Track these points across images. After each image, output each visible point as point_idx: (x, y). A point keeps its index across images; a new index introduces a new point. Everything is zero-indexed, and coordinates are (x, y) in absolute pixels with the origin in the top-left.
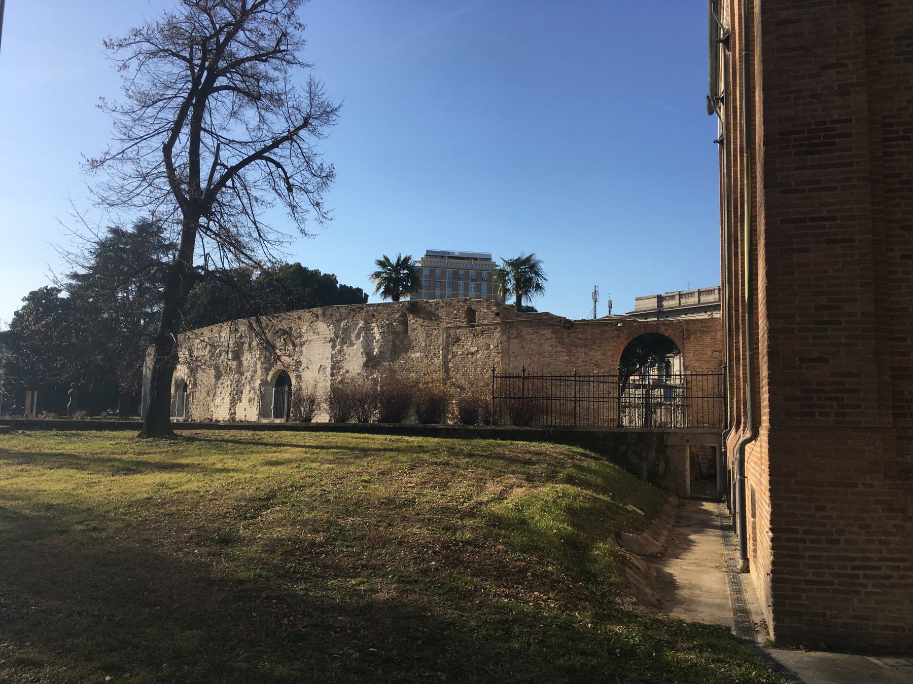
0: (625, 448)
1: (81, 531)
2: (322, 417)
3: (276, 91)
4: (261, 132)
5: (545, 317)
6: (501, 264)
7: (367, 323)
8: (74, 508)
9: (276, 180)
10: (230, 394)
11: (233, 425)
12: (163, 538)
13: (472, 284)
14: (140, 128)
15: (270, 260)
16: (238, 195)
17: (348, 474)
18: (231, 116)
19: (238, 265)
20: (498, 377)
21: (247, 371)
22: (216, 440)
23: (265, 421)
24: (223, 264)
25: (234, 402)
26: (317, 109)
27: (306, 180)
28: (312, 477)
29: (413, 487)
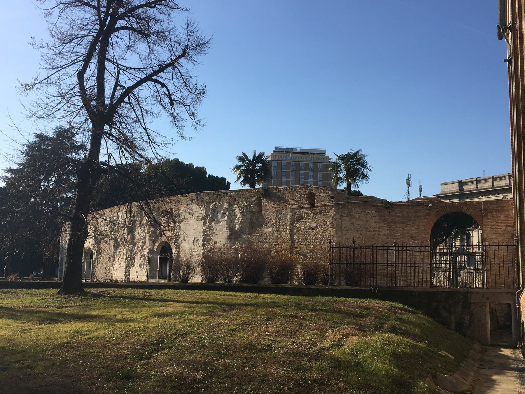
0: (436, 304)
1: (18, 368)
2: (196, 279)
3: (162, 30)
4: (150, 61)
5: (370, 200)
6: (334, 159)
7: (230, 205)
8: (12, 350)
9: (161, 96)
10: (126, 260)
11: (128, 284)
12: (80, 374)
13: (311, 174)
14: (60, 59)
15: (157, 158)
16: (133, 108)
17: (219, 324)
18: (128, 49)
19: (133, 161)
20: (334, 247)
21: (139, 243)
22: (116, 297)
23: (152, 281)
24: (122, 161)
25: (129, 266)
26: (193, 42)
27: (184, 96)
28: (191, 326)
29: (270, 335)
